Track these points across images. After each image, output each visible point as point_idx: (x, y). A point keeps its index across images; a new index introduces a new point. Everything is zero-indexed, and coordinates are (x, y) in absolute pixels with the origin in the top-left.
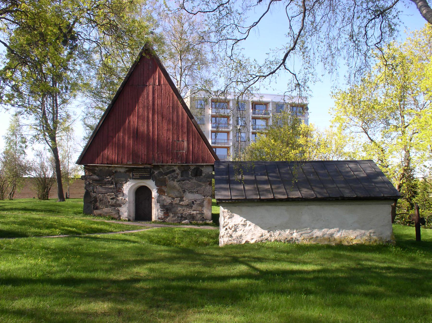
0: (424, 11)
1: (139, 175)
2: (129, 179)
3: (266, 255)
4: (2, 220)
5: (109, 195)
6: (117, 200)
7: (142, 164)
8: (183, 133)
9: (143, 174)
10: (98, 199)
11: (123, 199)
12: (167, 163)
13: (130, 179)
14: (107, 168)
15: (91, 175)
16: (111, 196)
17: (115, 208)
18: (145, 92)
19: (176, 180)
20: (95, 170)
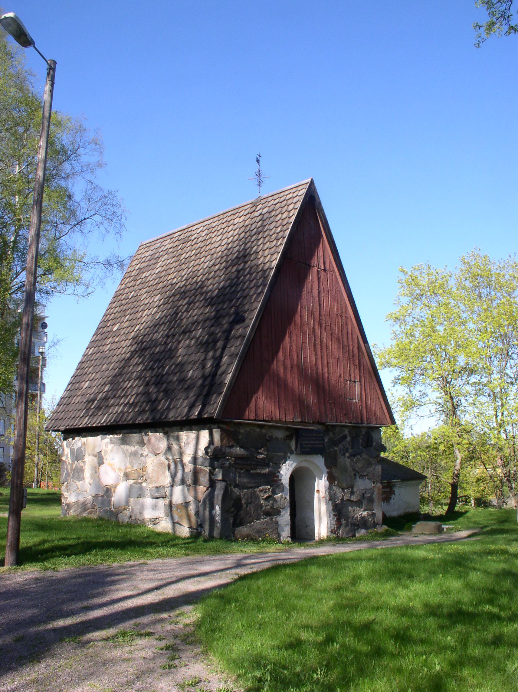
0: (226, 325)
1: (309, 446)
2: (289, 454)
3: (459, 577)
4: (514, 536)
5: (261, 491)
6: (275, 500)
7: (313, 423)
8: (354, 365)
9: (315, 444)
10: (243, 502)
11: (284, 496)
12: (341, 422)
13: (292, 453)
14: (258, 430)
15: (232, 446)
16: (265, 492)
17: (271, 519)
18: (315, 257)
19: (475, 439)
20: (239, 433)
